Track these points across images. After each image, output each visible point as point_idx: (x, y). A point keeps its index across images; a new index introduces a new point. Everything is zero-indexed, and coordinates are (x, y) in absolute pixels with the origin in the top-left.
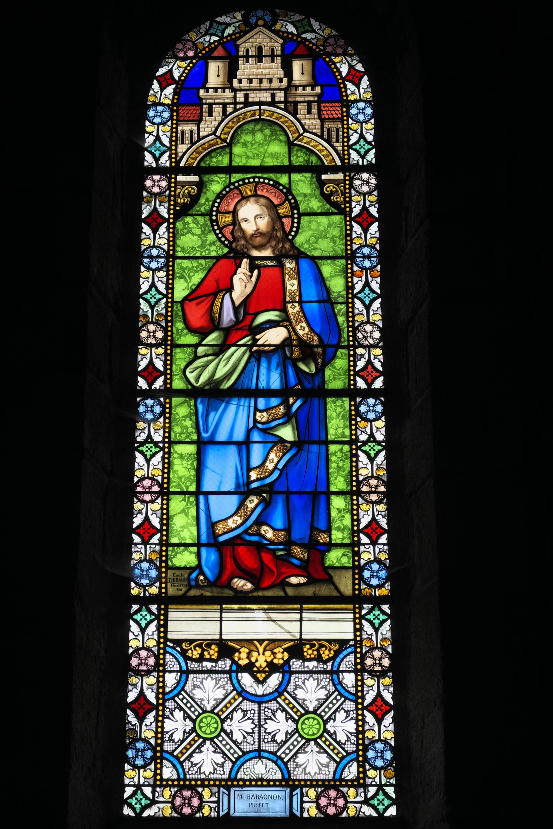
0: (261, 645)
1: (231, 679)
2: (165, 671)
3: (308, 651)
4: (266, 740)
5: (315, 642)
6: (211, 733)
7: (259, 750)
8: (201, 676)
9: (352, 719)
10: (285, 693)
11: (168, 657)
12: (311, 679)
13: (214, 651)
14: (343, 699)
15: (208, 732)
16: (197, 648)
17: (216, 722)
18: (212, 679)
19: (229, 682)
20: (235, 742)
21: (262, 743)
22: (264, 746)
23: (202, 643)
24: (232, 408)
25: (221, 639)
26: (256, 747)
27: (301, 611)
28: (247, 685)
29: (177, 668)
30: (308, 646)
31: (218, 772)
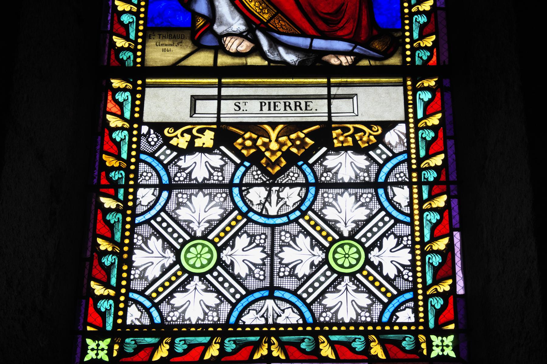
0: (274, 129)
1: (231, 194)
2: (137, 186)
3: (338, 137)
4: (281, 274)
5: (348, 125)
6: (203, 266)
7: (272, 289)
8: (189, 192)
9: (405, 247)
10: (310, 213)
11: (142, 167)
12: (346, 194)
13: (207, 139)
14: (392, 221)
15: (198, 265)
16: (185, 134)
17: (210, 251)
18: (205, 195)
19: (229, 199)
20: (236, 278)
21: (276, 278)
22: (277, 282)
23: (192, 129)
24: (233, 40)
25: (218, 123)
26: (267, 284)
27: (329, 85)
28: (255, 203)
29: (155, 181)
30: (339, 131)
31: (216, 178)
